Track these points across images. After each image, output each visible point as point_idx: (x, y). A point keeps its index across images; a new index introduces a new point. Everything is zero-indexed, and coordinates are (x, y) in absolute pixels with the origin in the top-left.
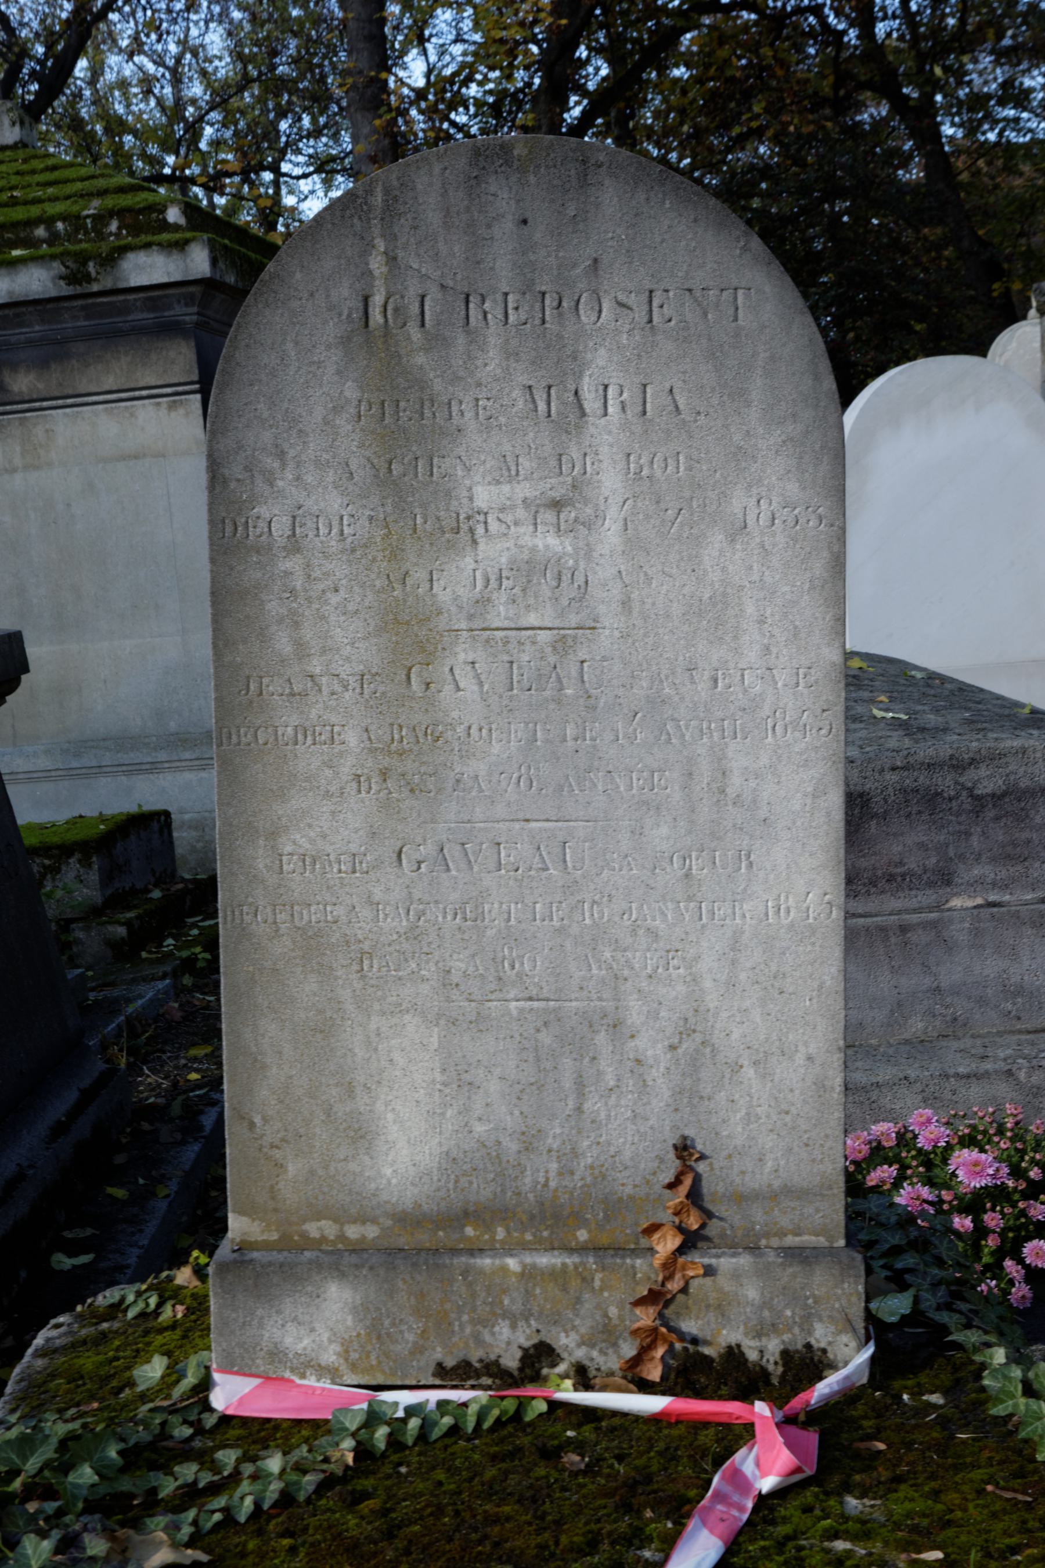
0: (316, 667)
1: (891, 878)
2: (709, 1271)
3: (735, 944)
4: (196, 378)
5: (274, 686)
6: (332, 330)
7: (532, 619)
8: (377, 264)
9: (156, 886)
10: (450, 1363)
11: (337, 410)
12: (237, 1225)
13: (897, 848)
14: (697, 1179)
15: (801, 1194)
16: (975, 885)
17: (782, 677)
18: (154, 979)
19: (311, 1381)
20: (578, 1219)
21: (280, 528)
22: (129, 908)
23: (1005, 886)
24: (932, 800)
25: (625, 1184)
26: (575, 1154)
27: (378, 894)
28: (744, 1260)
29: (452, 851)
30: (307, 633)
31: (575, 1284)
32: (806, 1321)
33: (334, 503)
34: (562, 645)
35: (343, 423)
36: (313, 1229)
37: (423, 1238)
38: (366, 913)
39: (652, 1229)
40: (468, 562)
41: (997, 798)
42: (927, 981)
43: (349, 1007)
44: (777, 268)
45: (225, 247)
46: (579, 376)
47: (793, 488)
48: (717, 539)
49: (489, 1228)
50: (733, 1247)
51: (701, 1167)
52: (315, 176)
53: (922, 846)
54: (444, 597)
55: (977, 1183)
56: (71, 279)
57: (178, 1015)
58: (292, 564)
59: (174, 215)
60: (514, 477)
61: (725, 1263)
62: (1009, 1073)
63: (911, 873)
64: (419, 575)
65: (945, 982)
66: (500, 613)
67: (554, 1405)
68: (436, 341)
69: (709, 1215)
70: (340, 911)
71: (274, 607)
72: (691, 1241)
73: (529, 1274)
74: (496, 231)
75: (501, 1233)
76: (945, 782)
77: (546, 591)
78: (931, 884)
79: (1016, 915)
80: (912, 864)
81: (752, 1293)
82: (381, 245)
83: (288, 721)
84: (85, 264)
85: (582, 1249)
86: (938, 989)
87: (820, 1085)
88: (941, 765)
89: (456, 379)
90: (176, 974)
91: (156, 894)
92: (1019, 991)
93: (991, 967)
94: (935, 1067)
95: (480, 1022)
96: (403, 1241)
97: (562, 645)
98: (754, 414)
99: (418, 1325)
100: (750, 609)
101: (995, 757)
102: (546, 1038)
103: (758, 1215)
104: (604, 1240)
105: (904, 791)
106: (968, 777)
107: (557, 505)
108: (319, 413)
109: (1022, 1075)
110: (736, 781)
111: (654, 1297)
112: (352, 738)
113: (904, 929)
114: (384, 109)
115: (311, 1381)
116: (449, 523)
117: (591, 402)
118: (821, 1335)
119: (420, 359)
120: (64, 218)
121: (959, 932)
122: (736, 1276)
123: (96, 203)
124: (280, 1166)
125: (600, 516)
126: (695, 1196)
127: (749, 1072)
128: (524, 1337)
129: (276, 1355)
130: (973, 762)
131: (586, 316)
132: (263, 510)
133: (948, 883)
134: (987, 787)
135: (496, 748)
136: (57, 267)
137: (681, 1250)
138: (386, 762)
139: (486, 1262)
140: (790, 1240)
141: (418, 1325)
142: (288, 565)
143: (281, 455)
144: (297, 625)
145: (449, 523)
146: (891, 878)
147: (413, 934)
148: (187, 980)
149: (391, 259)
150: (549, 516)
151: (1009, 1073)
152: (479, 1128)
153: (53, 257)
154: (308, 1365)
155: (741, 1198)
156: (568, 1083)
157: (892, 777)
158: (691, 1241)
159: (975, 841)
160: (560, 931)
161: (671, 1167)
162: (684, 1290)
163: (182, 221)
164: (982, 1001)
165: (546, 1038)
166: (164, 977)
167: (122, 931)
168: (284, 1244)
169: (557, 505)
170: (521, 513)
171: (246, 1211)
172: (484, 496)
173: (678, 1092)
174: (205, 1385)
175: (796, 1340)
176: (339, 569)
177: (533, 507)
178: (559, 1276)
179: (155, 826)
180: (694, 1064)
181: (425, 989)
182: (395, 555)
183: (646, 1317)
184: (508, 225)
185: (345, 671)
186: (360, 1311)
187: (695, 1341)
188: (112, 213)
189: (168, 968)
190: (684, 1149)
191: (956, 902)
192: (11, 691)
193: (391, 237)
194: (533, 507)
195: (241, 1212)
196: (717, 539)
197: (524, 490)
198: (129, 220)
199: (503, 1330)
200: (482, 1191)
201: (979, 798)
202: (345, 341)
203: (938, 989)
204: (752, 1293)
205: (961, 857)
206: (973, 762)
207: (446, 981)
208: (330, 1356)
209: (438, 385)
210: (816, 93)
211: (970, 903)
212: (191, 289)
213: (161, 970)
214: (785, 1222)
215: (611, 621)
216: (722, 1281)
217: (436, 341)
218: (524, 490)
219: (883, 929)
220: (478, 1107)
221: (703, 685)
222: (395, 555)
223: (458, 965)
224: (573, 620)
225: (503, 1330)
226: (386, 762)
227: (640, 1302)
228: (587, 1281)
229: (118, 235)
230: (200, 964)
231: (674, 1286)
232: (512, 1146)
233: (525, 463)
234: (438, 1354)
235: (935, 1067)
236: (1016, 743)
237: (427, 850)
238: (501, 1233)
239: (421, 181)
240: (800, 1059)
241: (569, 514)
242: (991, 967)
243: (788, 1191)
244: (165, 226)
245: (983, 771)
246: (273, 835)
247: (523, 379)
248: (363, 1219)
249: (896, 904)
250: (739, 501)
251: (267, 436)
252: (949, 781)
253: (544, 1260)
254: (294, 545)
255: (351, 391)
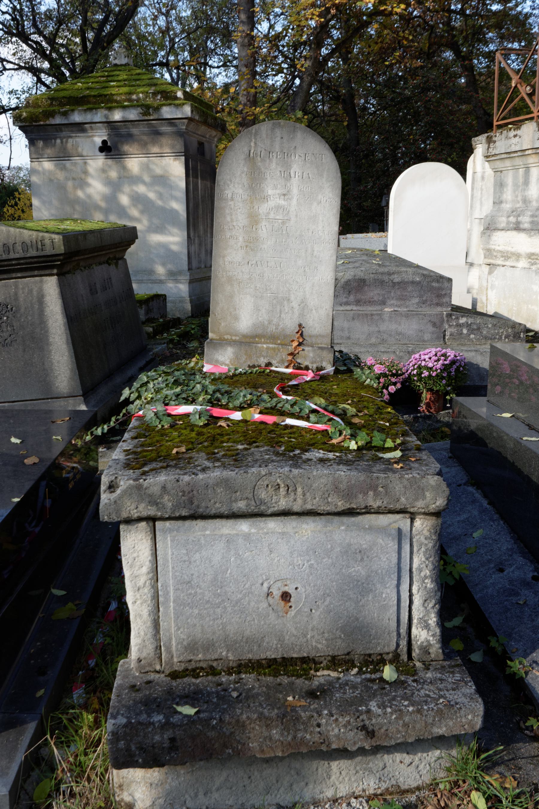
0: (235, 224)
1: (370, 302)
2: (303, 350)
3: (313, 286)
4: (183, 151)
5: (226, 227)
6: (243, 157)
7: (278, 217)
8: (252, 144)
9: (161, 318)
10: (251, 365)
11: (242, 173)
12: (211, 335)
13: (372, 294)
14: (302, 332)
15: (323, 336)
16: (392, 305)
17: (326, 232)
18: (161, 344)
19: (223, 367)
20: (278, 338)
21: (230, 196)
22: (153, 323)
23: (399, 306)
24: (382, 282)
25: (288, 332)
26: (279, 325)
27: (244, 270)
28: (310, 348)
29: (259, 263)
30: (233, 217)
31: (277, 351)
32: (322, 361)
33: (241, 191)
34: (283, 223)
35: (243, 175)
36: (226, 337)
37: (248, 340)
38: (241, 274)
39: (293, 341)
40: (266, 205)
41: (399, 283)
42: (377, 329)
43: (236, 293)
44: (331, 151)
45: (196, 107)
46: (290, 169)
47: (331, 195)
48: (315, 204)
49: (261, 339)
50: (308, 346)
51: (303, 330)
52: (222, 68)
53: (378, 294)
54: (261, 212)
55: (379, 372)
56: (144, 114)
57: (169, 355)
58: (231, 203)
59: (180, 94)
60: (276, 189)
61: (306, 349)
62: (394, 352)
63: (375, 301)
64: (256, 207)
65: (381, 329)
66: (272, 216)
67: (271, 371)
68: (263, 160)
69: (304, 339)
70: (236, 273)
71: (227, 211)
72: (300, 344)
73: (268, 348)
74: (276, 139)
75: (263, 340)
76: (386, 278)
77: (281, 212)
78: (380, 304)
79: (401, 314)
80: (375, 298)
81: (311, 355)
82: (253, 140)
83: (228, 234)
84: (149, 109)
85: (279, 344)
86: (379, 331)
87: (328, 315)
88: (385, 273)
89: (266, 168)
90: (168, 343)
91: (161, 320)
92: (400, 334)
93: (393, 327)
94: (376, 349)
95: (262, 297)
96: (243, 341)
97: (283, 223)
98: (324, 180)
99: (245, 357)
100: (321, 218)
101: (399, 273)
102: (274, 301)
103: (314, 340)
104: (283, 343)
105: (375, 279)
106: (392, 277)
107: (284, 195)
108: (239, 173)
109: (398, 353)
110: (315, 253)
111: (291, 354)
112: (241, 239)
113: (372, 315)
114: (252, 47)
115: (223, 367)
116: (263, 197)
117: (292, 175)
118: (324, 364)
119: (260, 164)
120: (142, 93)
121: (386, 317)
122: (308, 351)
123: (153, 88)
124: (220, 324)
125: (292, 198)
126: (302, 335)
127: (314, 311)
128: (266, 361)
129: (217, 361)
130: (393, 273)
131: (293, 158)
132: (226, 192)
133: (385, 304)
134: (396, 280)
135: (269, 243)
136: (139, 110)
137: (298, 345)
138: (247, 244)
139: (260, 345)
140: (320, 345)
141: (245, 357)
142: (230, 203)
143: (231, 181)
144: (231, 215)
145: (263, 197)
146: (370, 302)
147: (250, 279)
148: (171, 346)
149: (255, 144)
150: (282, 197)
151: (394, 352)
152: (260, 319)
153: (138, 106)
154: (223, 363)
155: (311, 336)
156: (278, 311)
157: (372, 276)
158: (300, 344)
159: (392, 294)
160: (279, 280)
161: (298, 329)
162: (298, 353)
163: (182, 97)
164: (390, 335)
165: (274, 301)
166: (164, 343)
167: (151, 329)
168: (220, 339)
169: (284, 195)
170: (277, 196)
171: (213, 332)
172: (270, 192)
173: (300, 314)
174: (203, 366)
175: (319, 365)
176: (241, 205)
177: (280, 195)
178: (274, 349)
179: (162, 299)
180: (303, 309)
181: (252, 290)
182: (252, 203)
183: (290, 358)
184: (279, 138)
185: (240, 225)
186: (234, 353)
187: (299, 364)
188: (159, 92)
189: (166, 341)
190: (300, 325)
191: (386, 309)
192: (133, 244)
193: (256, 139)
194: (280, 195)
195: (212, 332)
196: (315, 204)
197: (278, 191)
198: (164, 95)
199: (262, 359)
200: (260, 331)
201: (394, 283)
202: (245, 159)
203: (379, 331)
204: (311, 355)
205: (388, 298)
206: (393, 273)
207: (256, 289)
208: (228, 362)
209: (263, 169)
210: (421, 49)
211: (390, 310)
212: (184, 120)
213: (163, 342)
214: (319, 342)
215: (293, 219)
216: (305, 352)
217: (263, 160)
218: (278, 191)
219: (366, 315)
220: (260, 315)
221: (310, 233)
222: (252, 203)
223: (258, 286)
224: (286, 218)
225: (262, 359)
226: (247, 244)
227: (289, 354)
228: (279, 350)
229: (160, 100)
230: (175, 341)
231: (297, 352)
232: (266, 323)
233: (279, 186)
234: (249, 363)
235: (376, 349)
236: (405, 269)
237: (254, 262)
238: (263, 340)
239: (262, 128)
240: (324, 309)
241: (286, 197)
242: (393, 327)
243: (320, 335)
244: (176, 98)
245: (396, 276)
246: (224, 257)
247: (280, 169)
248: (236, 336)
249: (370, 308)
250: (320, 197)
251: (228, 177)
252: (387, 278)
253: (271, 346)
254: (232, 199)
255: (245, 169)
